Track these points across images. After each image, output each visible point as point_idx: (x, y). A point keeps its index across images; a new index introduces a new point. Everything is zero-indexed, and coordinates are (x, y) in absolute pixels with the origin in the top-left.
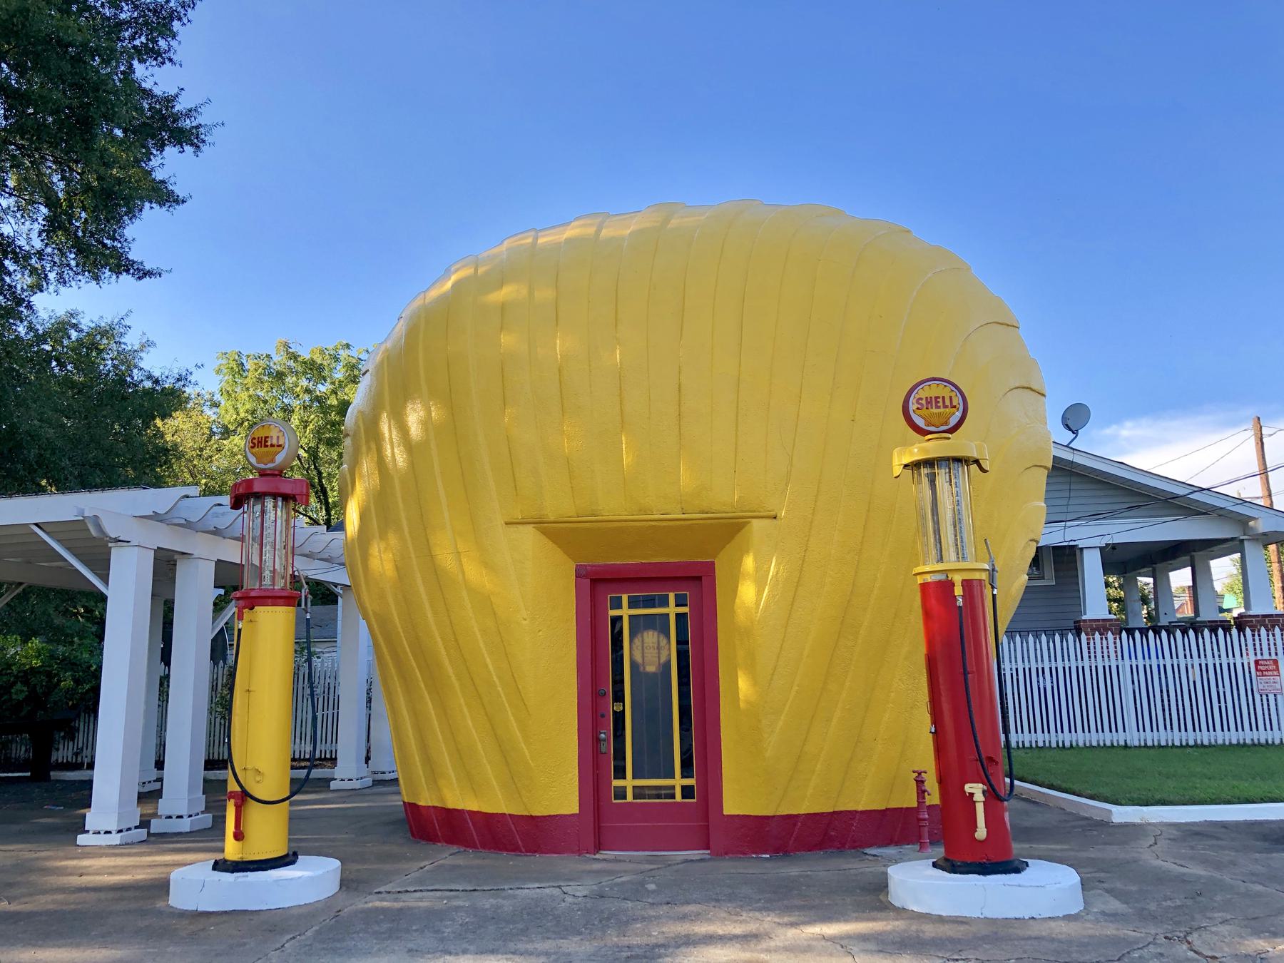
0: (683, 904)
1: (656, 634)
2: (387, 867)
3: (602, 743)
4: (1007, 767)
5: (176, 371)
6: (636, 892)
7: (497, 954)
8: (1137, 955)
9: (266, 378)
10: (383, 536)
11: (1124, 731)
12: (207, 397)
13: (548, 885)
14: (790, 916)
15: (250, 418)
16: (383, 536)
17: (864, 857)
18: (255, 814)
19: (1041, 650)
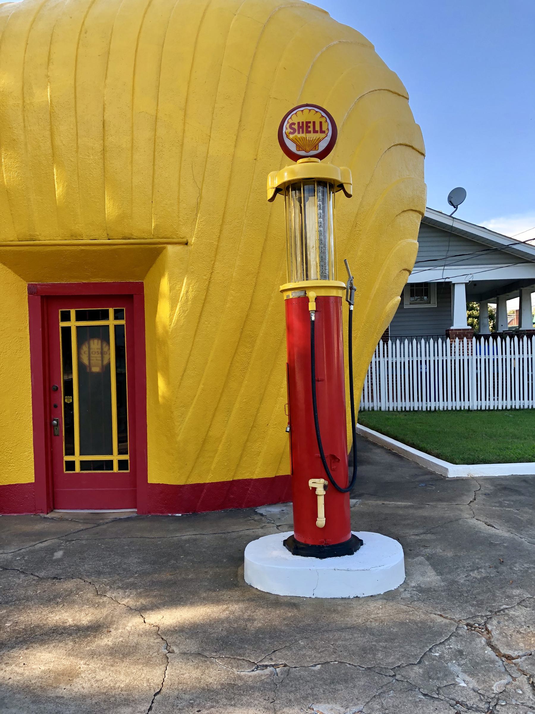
1: (100, 342)
8: (437, 654)
11: (469, 400)
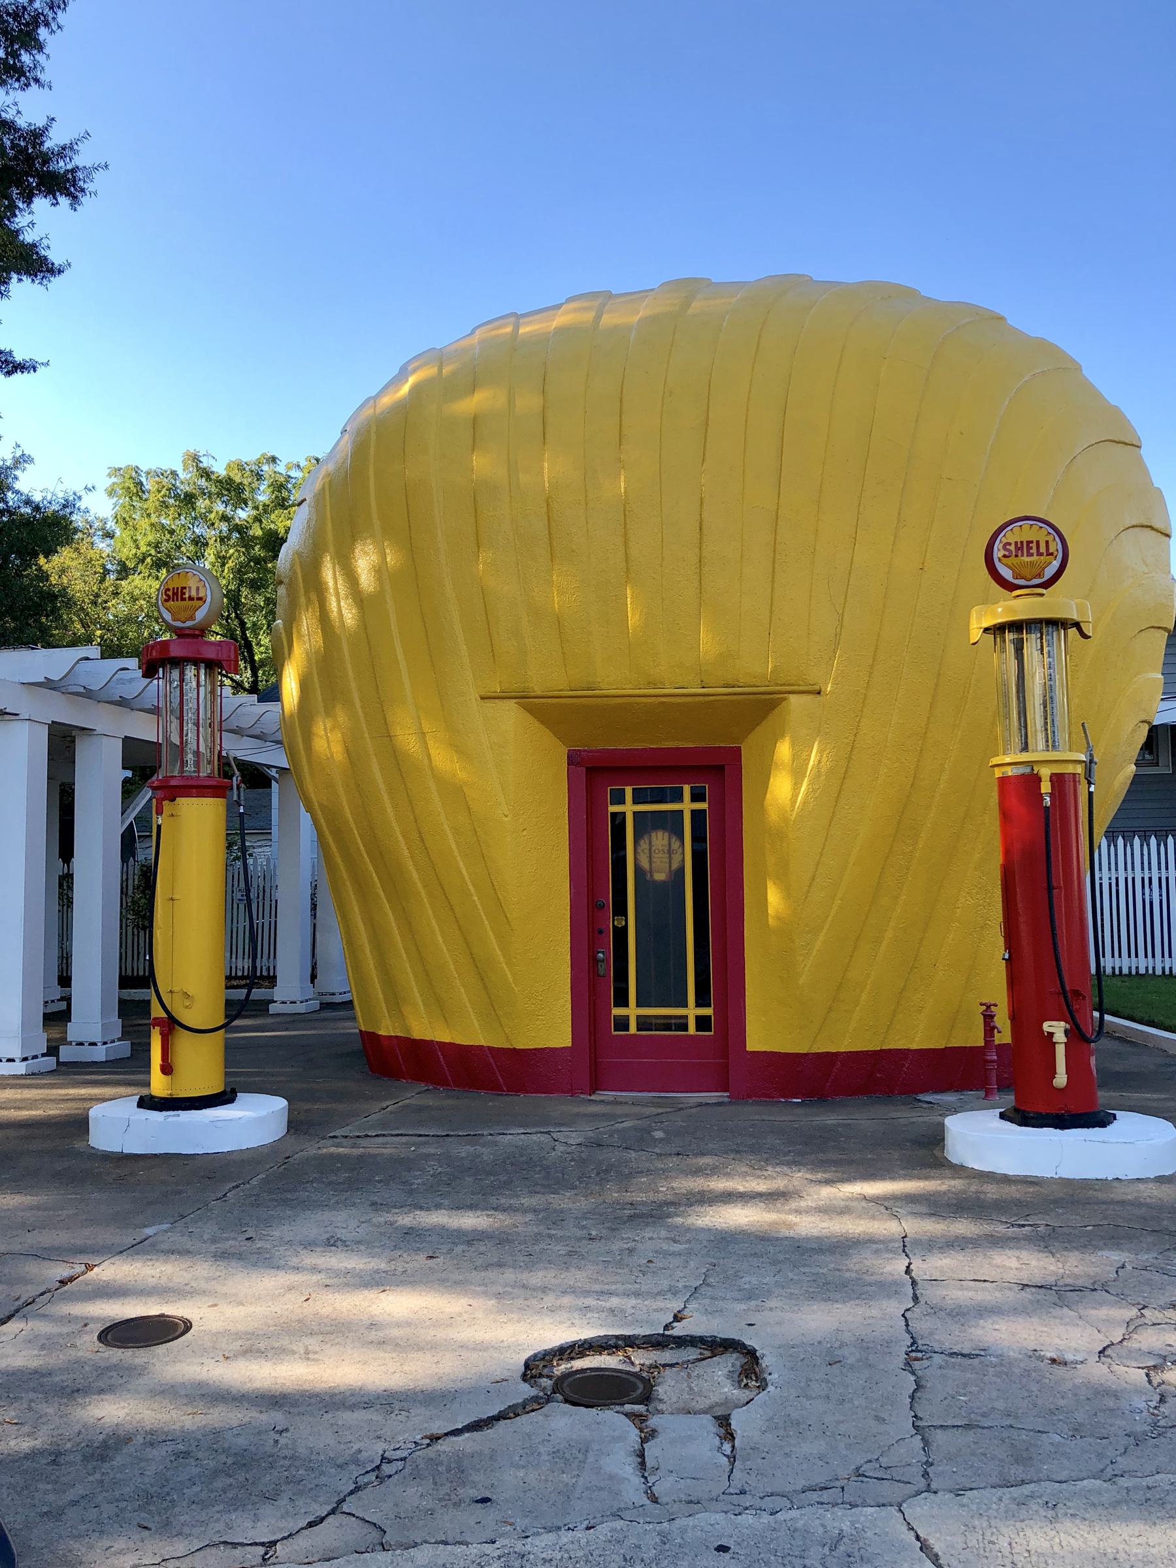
0: (696, 1155)
1: (666, 834)
2: (341, 1107)
3: (600, 964)
4: (1097, 999)
5: (61, 495)
6: (640, 1140)
7: (476, 1210)
9: (172, 501)
10: (329, 712)
12: (97, 524)
13: (534, 1130)
14: (824, 1172)
15: (153, 552)
16: (329, 712)
17: (916, 1104)
18: (184, 1044)
19: (1149, 854)
